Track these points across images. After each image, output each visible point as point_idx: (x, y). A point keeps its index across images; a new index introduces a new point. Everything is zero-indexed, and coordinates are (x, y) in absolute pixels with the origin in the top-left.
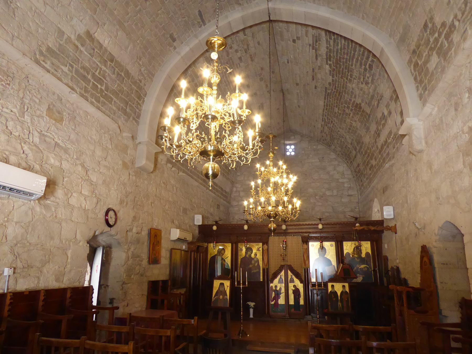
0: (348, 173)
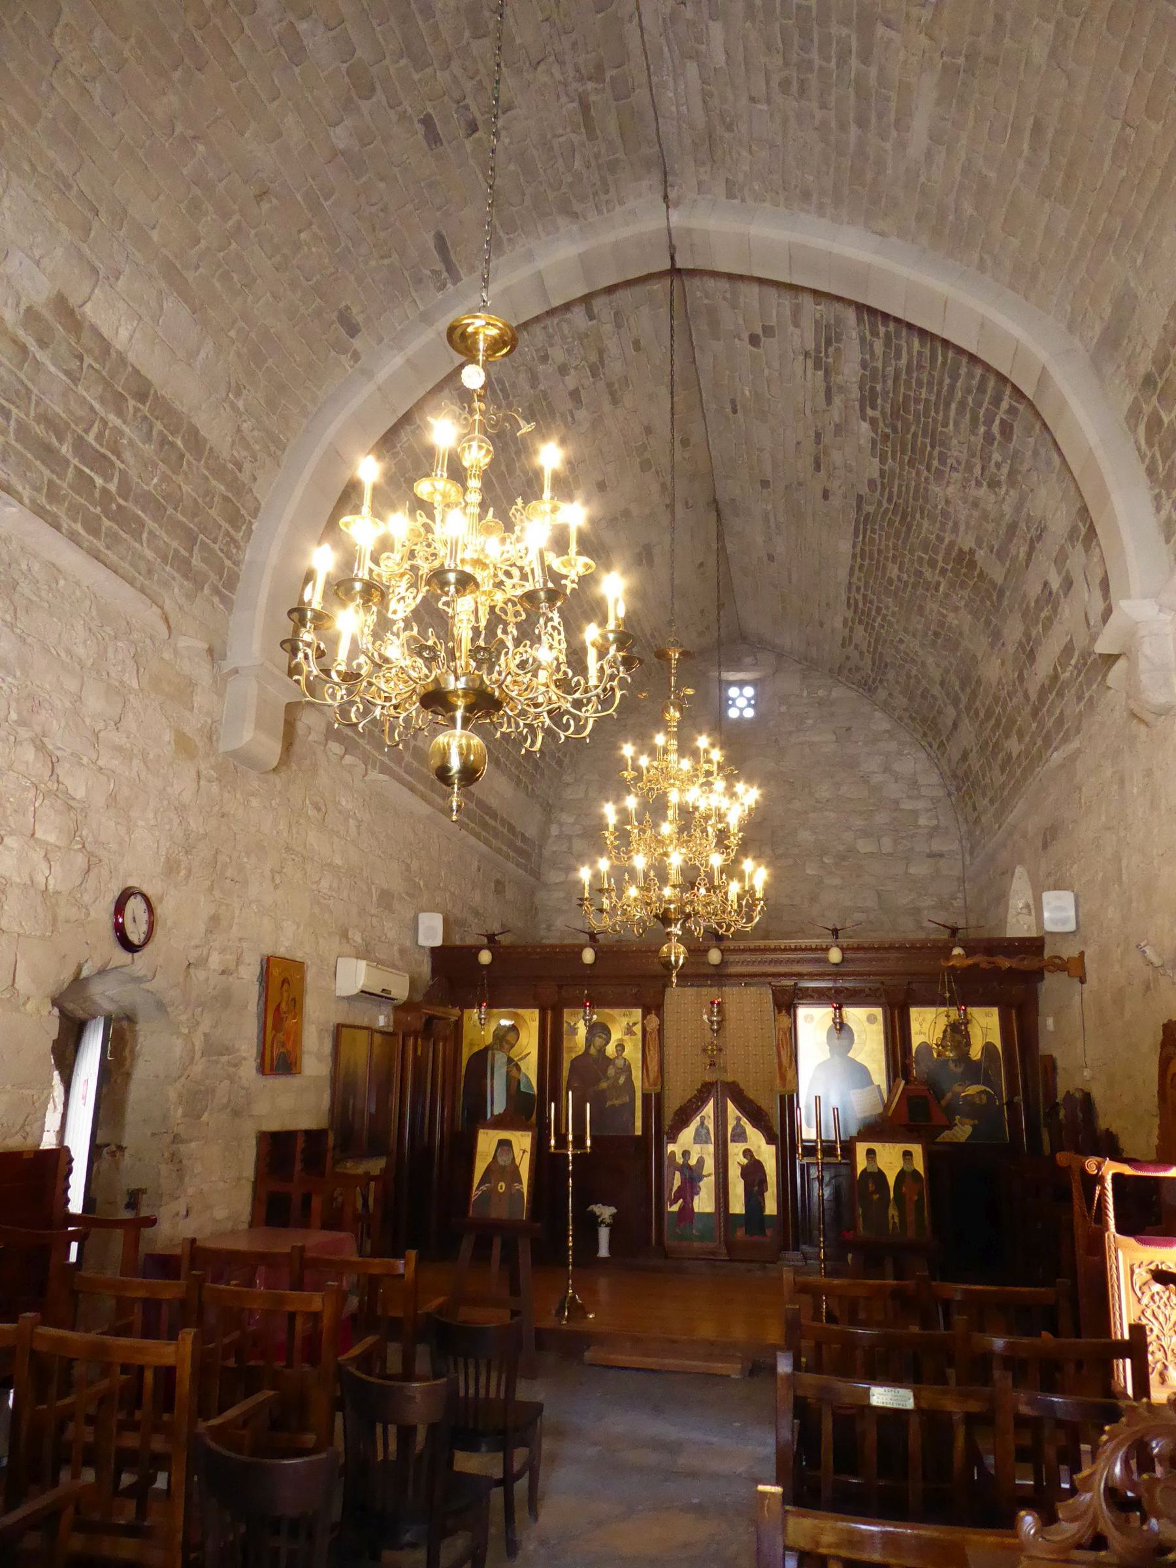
0: (930, 780)
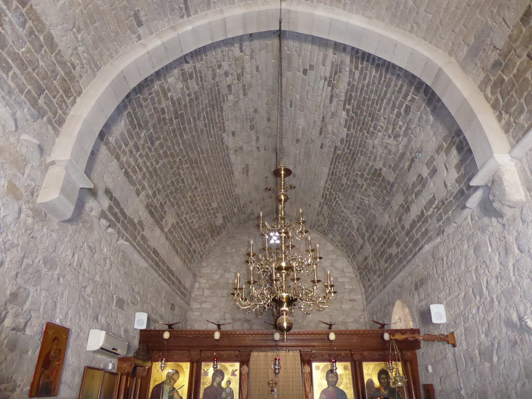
0: (350, 271)
